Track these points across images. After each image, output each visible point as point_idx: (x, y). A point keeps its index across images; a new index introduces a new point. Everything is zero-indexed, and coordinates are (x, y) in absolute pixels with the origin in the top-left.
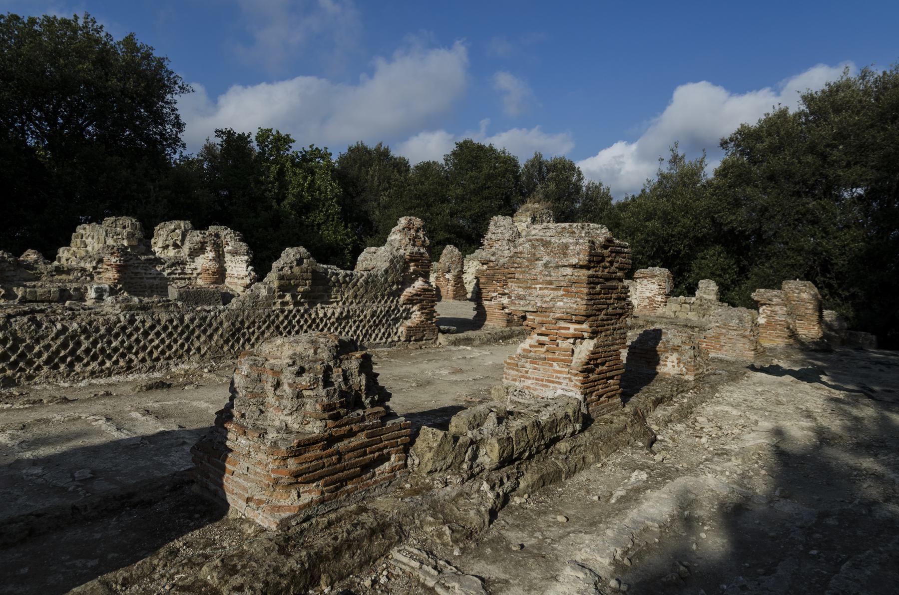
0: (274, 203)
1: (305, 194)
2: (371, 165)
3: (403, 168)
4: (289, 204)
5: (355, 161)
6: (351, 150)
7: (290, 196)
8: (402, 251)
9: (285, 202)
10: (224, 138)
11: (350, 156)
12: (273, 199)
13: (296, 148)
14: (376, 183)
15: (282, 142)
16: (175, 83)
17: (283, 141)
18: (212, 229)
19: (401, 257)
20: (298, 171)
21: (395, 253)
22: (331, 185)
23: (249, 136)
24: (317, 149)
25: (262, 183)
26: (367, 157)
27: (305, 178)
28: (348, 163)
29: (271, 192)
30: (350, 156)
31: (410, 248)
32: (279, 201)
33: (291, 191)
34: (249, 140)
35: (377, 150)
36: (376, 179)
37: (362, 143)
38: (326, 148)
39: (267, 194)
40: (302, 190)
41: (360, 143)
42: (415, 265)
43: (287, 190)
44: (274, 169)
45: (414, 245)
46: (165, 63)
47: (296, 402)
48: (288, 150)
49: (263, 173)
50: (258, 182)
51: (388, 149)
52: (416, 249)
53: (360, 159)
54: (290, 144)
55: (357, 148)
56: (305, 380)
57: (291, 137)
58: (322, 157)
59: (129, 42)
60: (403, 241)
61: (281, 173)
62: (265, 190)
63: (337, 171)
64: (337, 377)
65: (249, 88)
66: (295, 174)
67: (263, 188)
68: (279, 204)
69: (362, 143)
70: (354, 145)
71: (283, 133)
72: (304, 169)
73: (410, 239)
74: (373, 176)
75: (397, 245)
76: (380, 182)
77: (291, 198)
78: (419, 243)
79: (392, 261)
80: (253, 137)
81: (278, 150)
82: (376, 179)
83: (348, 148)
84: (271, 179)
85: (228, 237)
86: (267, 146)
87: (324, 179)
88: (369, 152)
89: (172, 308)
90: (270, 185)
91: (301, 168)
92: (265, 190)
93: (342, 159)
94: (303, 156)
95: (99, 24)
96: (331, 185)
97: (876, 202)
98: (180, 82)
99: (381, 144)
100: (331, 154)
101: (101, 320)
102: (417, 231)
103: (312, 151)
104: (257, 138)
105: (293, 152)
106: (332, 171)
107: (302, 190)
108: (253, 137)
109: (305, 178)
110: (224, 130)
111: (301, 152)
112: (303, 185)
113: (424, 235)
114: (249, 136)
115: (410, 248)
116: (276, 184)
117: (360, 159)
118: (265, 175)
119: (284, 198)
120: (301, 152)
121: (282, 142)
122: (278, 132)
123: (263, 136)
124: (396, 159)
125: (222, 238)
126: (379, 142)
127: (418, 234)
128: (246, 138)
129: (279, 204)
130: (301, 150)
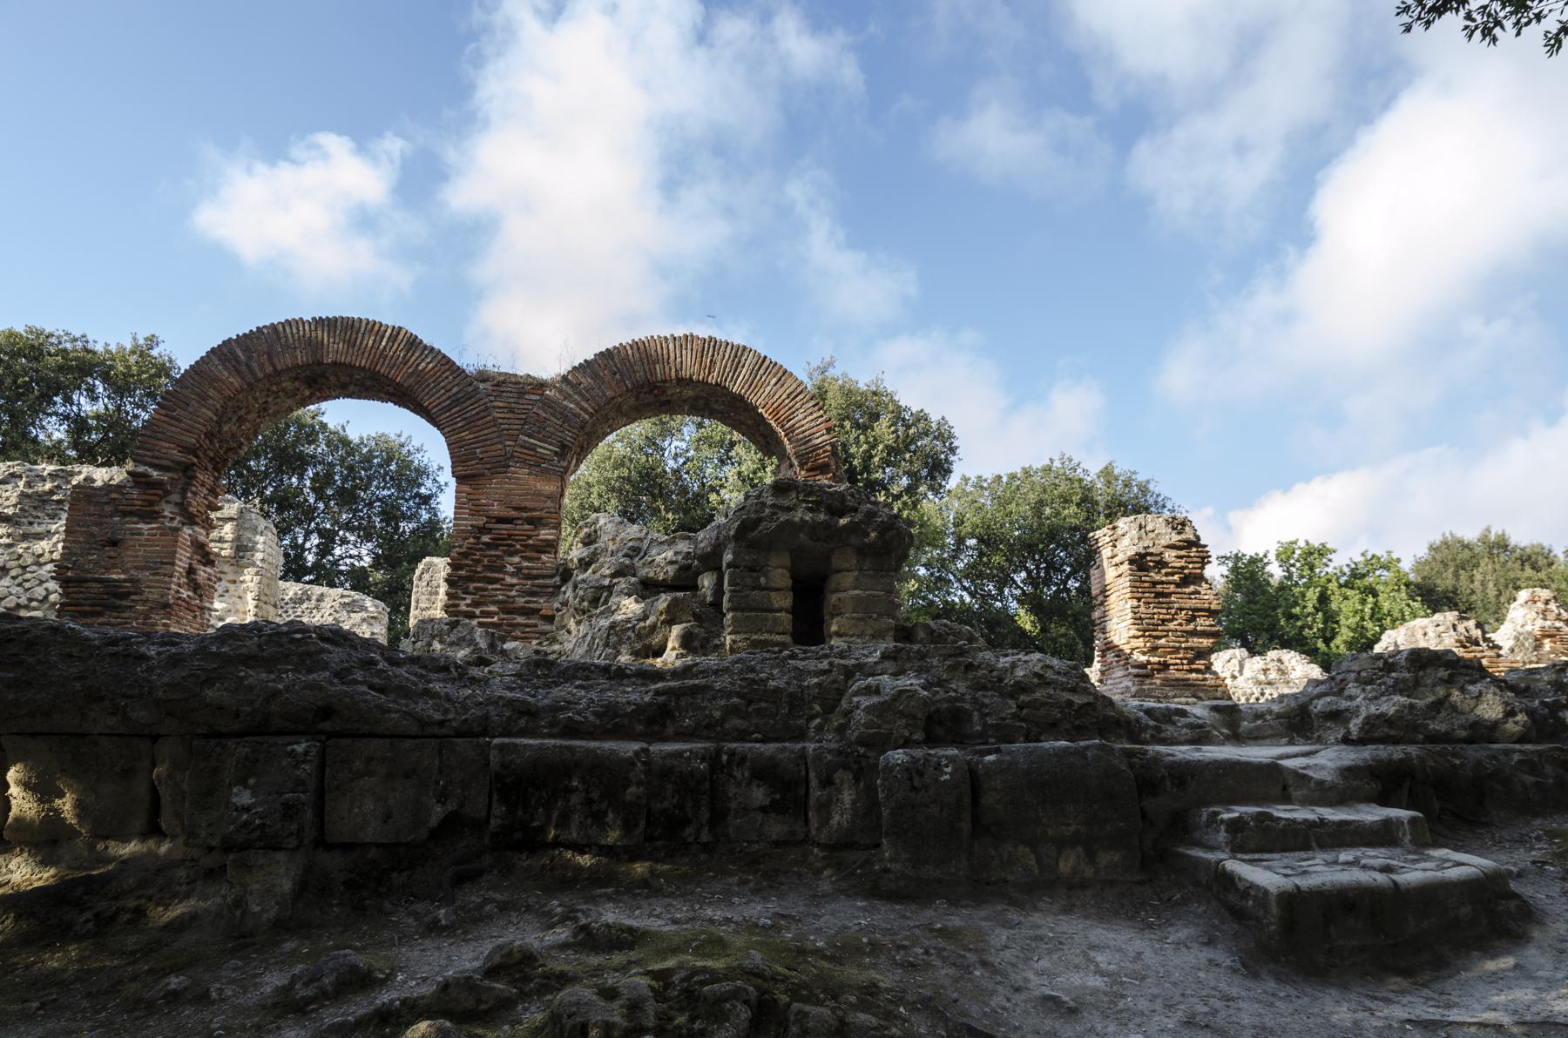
0: (1320, 644)
1: (1369, 624)
2: (1477, 565)
3: (1542, 562)
4: (1345, 642)
5: (1444, 564)
6: (1434, 549)
7: (1344, 630)
8: (1529, 628)
9: (1338, 641)
10: (1231, 565)
11: (1434, 558)
12: (1317, 638)
13: (1340, 561)
14: (1492, 591)
15: (1316, 555)
16: (1164, 506)
17: (1315, 555)
18: (1272, 654)
19: (1530, 633)
20: (1349, 592)
21: (1521, 630)
22: (1409, 605)
23: (1265, 556)
24: (1373, 556)
25: (1297, 618)
26: (1466, 554)
27: (1363, 602)
28: (1432, 569)
29: (1311, 628)
30: (1434, 558)
31: (1540, 623)
32: (1327, 641)
33: (1343, 621)
34: (1266, 561)
35: (1484, 540)
36: (1491, 585)
37: (1452, 534)
38: (1389, 553)
39: (1306, 632)
40: (1363, 619)
41: (1448, 535)
42: (1551, 642)
43: (1337, 622)
44: (1312, 595)
45: (1545, 619)
46: (1151, 487)
47: (1438, 640)
48: (1327, 566)
49: (1296, 604)
50: (1290, 617)
51: (1503, 535)
52: (1548, 623)
53: (1454, 559)
54: (1330, 556)
55: (1445, 543)
56: (1441, 629)
57: (1328, 546)
58: (1386, 567)
59: (1107, 473)
60: (1529, 616)
61: (1324, 599)
62: (1302, 628)
63: (1418, 586)
64: (1461, 628)
65: (1299, 487)
66: (1346, 598)
67: (1299, 623)
68: (1328, 646)
69: (1452, 534)
70: (1438, 539)
71: (1316, 543)
72: (1359, 588)
73: (1537, 613)
74: (1483, 584)
75: (1520, 621)
76: (1499, 590)
77: (1344, 634)
78: (1551, 616)
79: (1517, 639)
80: (1272, 556)
81: (1312, 568)
82: (1491, 585)
83: (1427, 546)
84: (1310, 609)
85: (1293, 661)
86: (1293, 565)
87: (1395, 600)
88: (1467, 547)
89: (1291, 684)
90: (1309, 619)
91: (1352, 588)
92: (1302, 628)
93: (1419, 565)
94: (1352, 570)
95: (1075, 462)
96: (1409, 605)
97: (377, 563)
98: (1169, 506)
99: (1488, 530)
100: (1399, 560)
101: (1240, 692)
102: (1547, 602)
103: (1366, 560)
104: (1278, 556)
105: (1335, 568)
106: (1407, 585)
107: (1363, 619)
108: (1272, 556)
109: (1363, 602)
110: (1228, 555)
111: (1348, 566)
112: (1362, 611)
113: (1558, 607)
114: (1265, 556)
115: (1540, 623)
116: (1320, 615)
117: (1454, 559)
118: (1299, 605)
119: (1334, 635)
120: (1348, 566)
121: (1316, 555)
122: (1307, 543)
123: (1285, 554)
124: (1523, 549)
125: (1286, 663)
126: (1485, 526)
127: (1549, 607)
128: (1261, 560)
129: (1328, 646)
130: (1348, 562)
